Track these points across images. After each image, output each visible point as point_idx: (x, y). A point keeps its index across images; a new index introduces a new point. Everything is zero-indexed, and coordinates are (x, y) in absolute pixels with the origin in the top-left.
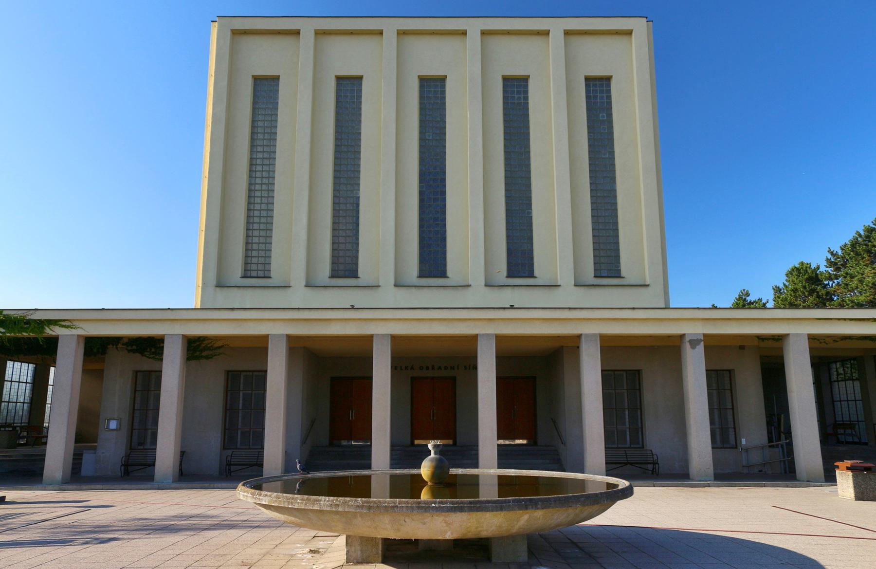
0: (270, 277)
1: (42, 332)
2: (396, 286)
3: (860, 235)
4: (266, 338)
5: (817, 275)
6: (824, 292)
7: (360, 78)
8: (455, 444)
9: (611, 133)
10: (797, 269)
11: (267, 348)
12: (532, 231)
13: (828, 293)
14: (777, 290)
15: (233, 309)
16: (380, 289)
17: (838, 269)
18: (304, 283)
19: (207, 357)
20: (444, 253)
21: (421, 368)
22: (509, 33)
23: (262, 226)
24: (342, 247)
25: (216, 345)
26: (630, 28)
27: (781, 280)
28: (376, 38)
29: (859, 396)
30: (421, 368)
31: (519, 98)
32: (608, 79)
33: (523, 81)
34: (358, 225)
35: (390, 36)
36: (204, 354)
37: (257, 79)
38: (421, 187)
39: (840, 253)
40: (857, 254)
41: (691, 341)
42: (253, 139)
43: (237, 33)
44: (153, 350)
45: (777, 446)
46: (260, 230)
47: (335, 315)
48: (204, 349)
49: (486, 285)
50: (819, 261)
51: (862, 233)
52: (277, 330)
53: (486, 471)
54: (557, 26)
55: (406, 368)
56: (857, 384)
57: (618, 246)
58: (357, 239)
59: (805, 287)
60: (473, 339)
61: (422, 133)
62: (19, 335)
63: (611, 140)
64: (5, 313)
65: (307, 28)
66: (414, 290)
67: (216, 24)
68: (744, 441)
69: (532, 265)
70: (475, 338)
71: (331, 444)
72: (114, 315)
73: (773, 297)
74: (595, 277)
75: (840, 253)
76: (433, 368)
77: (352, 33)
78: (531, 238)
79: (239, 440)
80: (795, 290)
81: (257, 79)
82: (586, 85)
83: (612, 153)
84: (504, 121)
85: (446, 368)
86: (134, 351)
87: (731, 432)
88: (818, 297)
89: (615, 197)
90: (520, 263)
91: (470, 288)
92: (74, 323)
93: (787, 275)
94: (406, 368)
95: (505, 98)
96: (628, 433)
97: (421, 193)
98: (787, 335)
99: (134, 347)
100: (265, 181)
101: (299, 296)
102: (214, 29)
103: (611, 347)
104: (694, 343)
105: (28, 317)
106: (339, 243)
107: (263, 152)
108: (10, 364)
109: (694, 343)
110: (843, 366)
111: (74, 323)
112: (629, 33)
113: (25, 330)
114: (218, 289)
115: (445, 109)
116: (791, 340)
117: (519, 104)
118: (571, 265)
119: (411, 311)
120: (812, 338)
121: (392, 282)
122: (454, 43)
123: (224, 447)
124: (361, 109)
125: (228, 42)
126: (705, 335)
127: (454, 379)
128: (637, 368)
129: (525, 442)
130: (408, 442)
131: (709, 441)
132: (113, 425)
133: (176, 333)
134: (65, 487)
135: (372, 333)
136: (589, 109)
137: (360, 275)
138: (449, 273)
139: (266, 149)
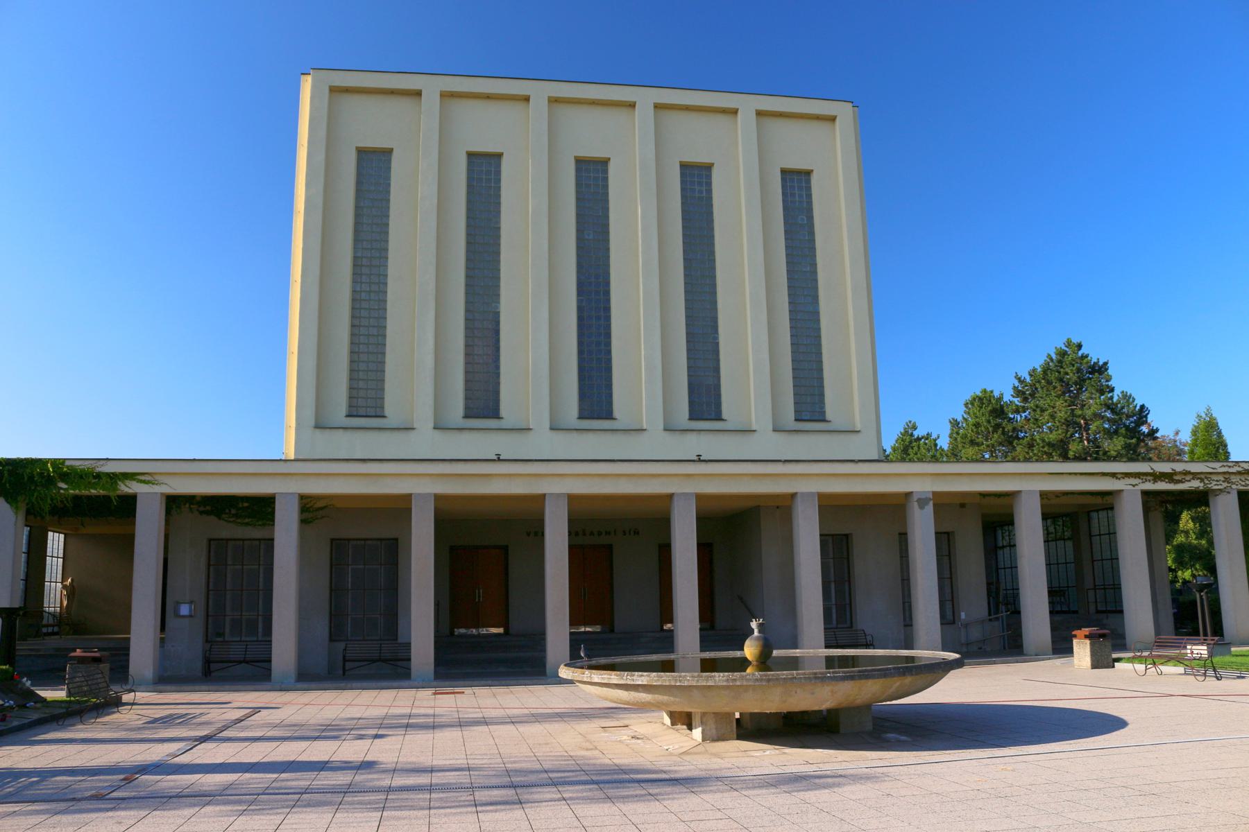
0: (384, 417)
1: (115, 489)
2: (551, 429)
3: (1051, 359)
4: (408, 498)
5: (1002, 407)
6: (1009, 427)
8: (507, 633)
9: (812, 241)
10: (981, 399)
11: (410, 509)
13: (1014, 429)
14: (955, 423)
15: (364, 460)
17: (1025, 400)
18: (432, 425)
22: (687, 108)
26: (833, 113)
27: (959, 413)
28: (519, 106)
29: (1071, 557)
31: (701, 192)
32: (808, 173)
34: (498, 349)
38: (579, 302)
39: (1028, 379)
40: (1049, 383)
41: (919, 500)
44: (233, 511)
45: (997, 619)
46: (368, 353)
49: (665, 430)
50: (1005, 390)
51: (1054, 357)
52: (422, 486)
53: (810, 652)
56: (1069, 544)
59: (989, 422)
61: (579, 231)
62: (85, 492)
63: (813, 249)
64: (67, 463)
66: (575, 434)
67: (309, 78)
68: (963, 615)
70: (670, 496)
72: (210, 468)
73: (948, 432)
75: (1028, 379)
76: (584, 534)
78: (717, 370)
80: (977, 425)
83: (814, 265)
88: (1003, 433)
89: (818, 321)
90: (705, 402)
92: (157, 477)
93: (966, 405)
96: (834, 611)
97: (580, 309)
98: (1019, 492)
99: (208, 508)
100: (374, 288)
101: (425, 442)
103: (831, 506)
104: (922, 503)
105: (98, 470)
108: (50, 534)
110: (1054, 523)
111: (157, 477)
112: (833, 119)
113: (94, 486)
116: (1023, 497)
118: (769, 406)
120: (1044, 495)
121: (548, 426)
122: (619, 115)
123: (332, 639)
126: (934, 493)
127: (609, 548)
128: (858, 527)
129: (598, 629)
131: (938, 616)
132: (185, 610)
134: (161, 687)
136: (785, 208)
138: (616, 413)
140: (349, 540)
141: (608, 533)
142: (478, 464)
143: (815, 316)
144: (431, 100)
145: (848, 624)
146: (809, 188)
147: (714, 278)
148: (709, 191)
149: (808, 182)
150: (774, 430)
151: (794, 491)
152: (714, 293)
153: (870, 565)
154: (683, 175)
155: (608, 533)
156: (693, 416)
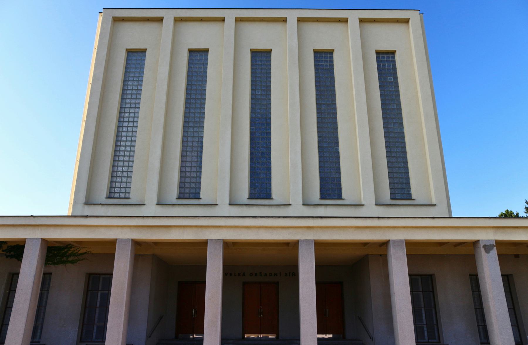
7: (206, 51)
8: (278, 338)
12: (339, 163)
16: (217, 207)
19: (72, 262)
20: (270, 179)
21: (251, 275)
23: (127, 159)
24: (188, 175)
25: (82, 251)
30: (251, 275)
32: (393, 53)
33: (330, 53)
35: (230, 22)
36: (70, 259)
37: (191, 52)
38: (251, 129)
41: (485, 247)
42: (123, 94)
43: (117, 20)
47: (180, 226)
48: (70, 255)
54: (354, 16)
55: (239, 275)
57: (408, 175)
58: (201, 168)
60: (294, 245)
65: (169, 18)
66: (245, 207)
67: (102, 14)
69: (341, 189)
71: (177, 337)
74: (391, 199)
76: (261, 275)
77: (202, 20)
79: (94, 334)
81: (191, 52)
82: (377, 57)
83: (399, 105)
84: (316, 81)
85: (271, 275)
86: (11, 257)
87: (39, 331)
89: (403, 138)
91: (291, 207)
94: (239, 275)
95: (316, 65)
96: (425, 329)
99: (12, 253)
101: (152, 209)
102: (100, 18)
103: (417, 252)
104: (488, 248)
106: (185, 172)
107: (131, 103)
109: (488, 248)
112: (406, 21)
114: (86, 206)
115: (270, 73)
117: (327, 70)
118: (373, 189)
119: (241, 219)
121: (228, 202)
122: (277, 27)
124: (206, 72)
125: (110, 26)
127: (277, 283)
129: (331, 336)
130: (241, 336)
133: (36, 237)
135: (207, 238)
136: (379, 74)
137: (201, 196)
139: (133, 101)
140: (100, 274)
141: (276, 275)
142: (162, 219)
143: (401, 134)
144: (169, 22)
145: (437, 340)
146: (394, 61)
147: (335, 114)
148: (332, 65)
149: (394, 57)
150: (376, 205)
151: (388, 238)
152: (336, 123)
153: (450, 295)
154: (315, 57)
155: (276, 275)
156: (323, 197)
